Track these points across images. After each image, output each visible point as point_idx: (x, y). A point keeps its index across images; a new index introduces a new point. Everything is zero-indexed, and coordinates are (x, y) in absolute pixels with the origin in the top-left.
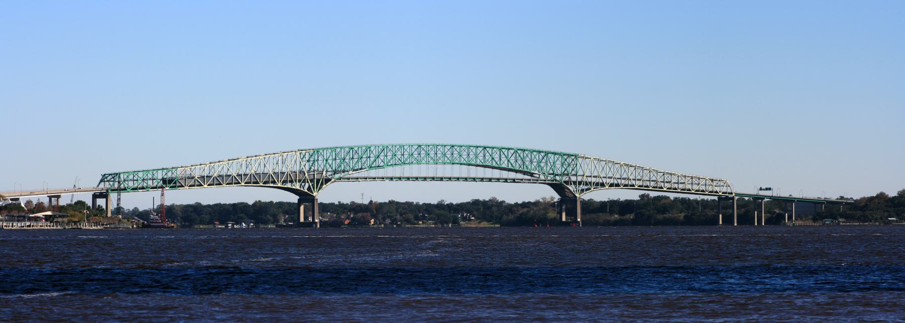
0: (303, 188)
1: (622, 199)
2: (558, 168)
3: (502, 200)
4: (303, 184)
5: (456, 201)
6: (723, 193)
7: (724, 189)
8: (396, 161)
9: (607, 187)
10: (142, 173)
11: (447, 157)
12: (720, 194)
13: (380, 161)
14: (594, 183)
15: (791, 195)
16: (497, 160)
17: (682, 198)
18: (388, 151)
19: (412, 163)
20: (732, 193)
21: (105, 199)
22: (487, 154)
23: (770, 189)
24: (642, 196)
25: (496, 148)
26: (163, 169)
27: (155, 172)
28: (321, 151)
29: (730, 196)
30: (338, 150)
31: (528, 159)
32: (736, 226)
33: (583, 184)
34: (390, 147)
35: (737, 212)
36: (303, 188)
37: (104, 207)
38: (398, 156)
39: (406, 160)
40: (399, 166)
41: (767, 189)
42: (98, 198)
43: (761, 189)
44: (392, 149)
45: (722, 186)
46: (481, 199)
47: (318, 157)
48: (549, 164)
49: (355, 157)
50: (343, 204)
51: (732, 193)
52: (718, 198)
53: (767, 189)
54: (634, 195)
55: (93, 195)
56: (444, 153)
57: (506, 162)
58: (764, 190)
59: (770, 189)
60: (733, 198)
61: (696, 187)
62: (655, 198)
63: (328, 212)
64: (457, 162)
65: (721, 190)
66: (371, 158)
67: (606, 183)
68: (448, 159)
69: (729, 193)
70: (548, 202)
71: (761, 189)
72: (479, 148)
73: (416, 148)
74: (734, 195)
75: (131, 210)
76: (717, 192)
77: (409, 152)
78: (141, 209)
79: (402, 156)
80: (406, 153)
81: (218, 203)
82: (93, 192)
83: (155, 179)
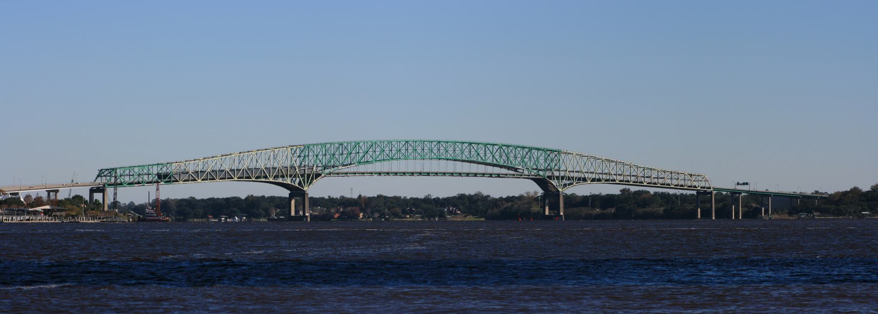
0: (294, 182)
1: (604, 193)
3: (487, 195)
4: (294, 179)
5: (442, 195)
6: (701, 188)
7: (703, 184)
9: (589, 182)
11: (433, 152)
12: (699, 188)
13: (369, 156)
14: (576, 178)
15: (767, 190)
18: (376, 146)
20: (710, 188)
21: (102, 194)
23: (747, 184)
25: (481, 144)
26: (158, 164)
27: (150, 167)
29: (709, 190)
30: (328, 146)
31: (512, 155)
32: (714, 220)
34: (378, 143)
37: (101, 201)
40: (387, 162)
41: (744, 184)
42: (95, 192)
43: (738, 184)
46: (467, 194)
51: (710, 188)
52: (697, 193)
53: (744, 184)
54: (615, 190)
55: (90, 190)
57: (491, 158)
58: (741, 184)
59: (747, 184)
60: (711, 193)
61: (675, 182)
64: (443, 157)
65: (700, 184)
67: (588, 178)
68: (435, 154)
69: (707, 188)
71: (738, 184)
72: (464, 144)
74: (712, 189)
76: (695, 187)
78: (137, 204)
79: (390, 152)
80: (394, 149)
82: (90, 187)
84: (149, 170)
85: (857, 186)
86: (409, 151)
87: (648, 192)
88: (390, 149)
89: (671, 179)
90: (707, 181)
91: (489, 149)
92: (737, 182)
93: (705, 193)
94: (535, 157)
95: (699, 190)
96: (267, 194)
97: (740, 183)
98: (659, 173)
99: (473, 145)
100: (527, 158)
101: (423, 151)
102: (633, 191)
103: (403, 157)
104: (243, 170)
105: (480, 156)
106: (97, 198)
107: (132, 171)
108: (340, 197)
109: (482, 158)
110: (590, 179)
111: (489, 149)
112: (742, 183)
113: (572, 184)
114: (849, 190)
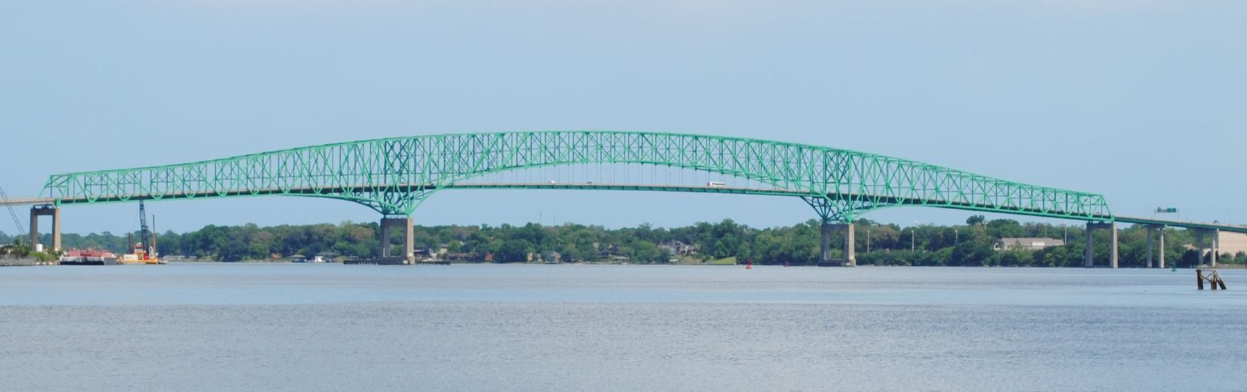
0: (390, 200)
1: (938, 224)
2: (819, 171)
3: (742, 224)
4: (389, 194)
6: (1094, 216)
7: (1096, 210)
8: (575, 156)
9: (900, 203)
10: (180, 168)
11: (659, 154)
12: (1091, 217)
13: (520, 157)
14: (877, 198)
15: (1215, 222)
16: (716, 157)
17: (1038, 225)
18: (589, 139)
19: (546, 163)
20: (1109, 217)
21: (51, 217)
22: (726, 151)
23: (1174, 210)
24: (972, 221)
27: (202, 166)
28: (420, 140)
29: (1107, 221)
31: (768, 157)
33: (860, 199)
34: (536, 134)
35: (1165, 254)
36: (390, 200)
37: (1087, 222)
38: (605, 148)
39: (481, 161)
40: (552, 166)
41: (1169, 210)
42: (40, 214)
43: (1159, 210)
44: (539, 137)
45: (1094, 204)
47: (531, 144)
48: (803, 165)
49: (478, 150)
50: (490, 229)
52: (1088, 224)
53: (1169, 210)
55: (32, 210)
56: (627, 146)
57: (730, 162)
58: (1164, 211)
59: (1174, 210)
60: (1110, 226)
61: (1049, 206)
62: (993, 222)
63: (886, 248)
64: (648, 160)
65: (1091, 210)
66: (137, 177)
67: (898, 198)
68: (662, 156)
69: (1105, 217)
70: (1079, 228)
71: (1159, 210)
72: (686, 138)
73: (580, 137)
74: (1113, 219)
75: (652, 228)
76: (1084, 215)
77: (567, 142)
78: (612, 230)
79: (585, 149)
80: (562, 144)
81: (283, 224)
82: (31, 206)
83: (137, 183)
84: (200, 172)
85: (505, 222)
86: (616, 148)
87: (1016, 223)
88: (640, 145)
89: (167, 182)
90: (1105, 204)
91: (647, 140)
92: (1157, 208)
93: (1101, 225)
94: (807, 160)
95: (1089, 220)
96: (995, 219)
97: (1163, 208)
98: (1022, 190)
99: (726, 142)
100: (793, 163)
101: (668, 152)
102: (990, 220)
103: (606, 159)
104: (861, 196)
105: (739, 163)
106: (965, 221)
107: (105, 178)
108: (503, 226)
109: (715, 163)
110: (319, 189)
111: (727, 146)
112: (1166, 208)
113: (871, 207)
114: (762, 230)
